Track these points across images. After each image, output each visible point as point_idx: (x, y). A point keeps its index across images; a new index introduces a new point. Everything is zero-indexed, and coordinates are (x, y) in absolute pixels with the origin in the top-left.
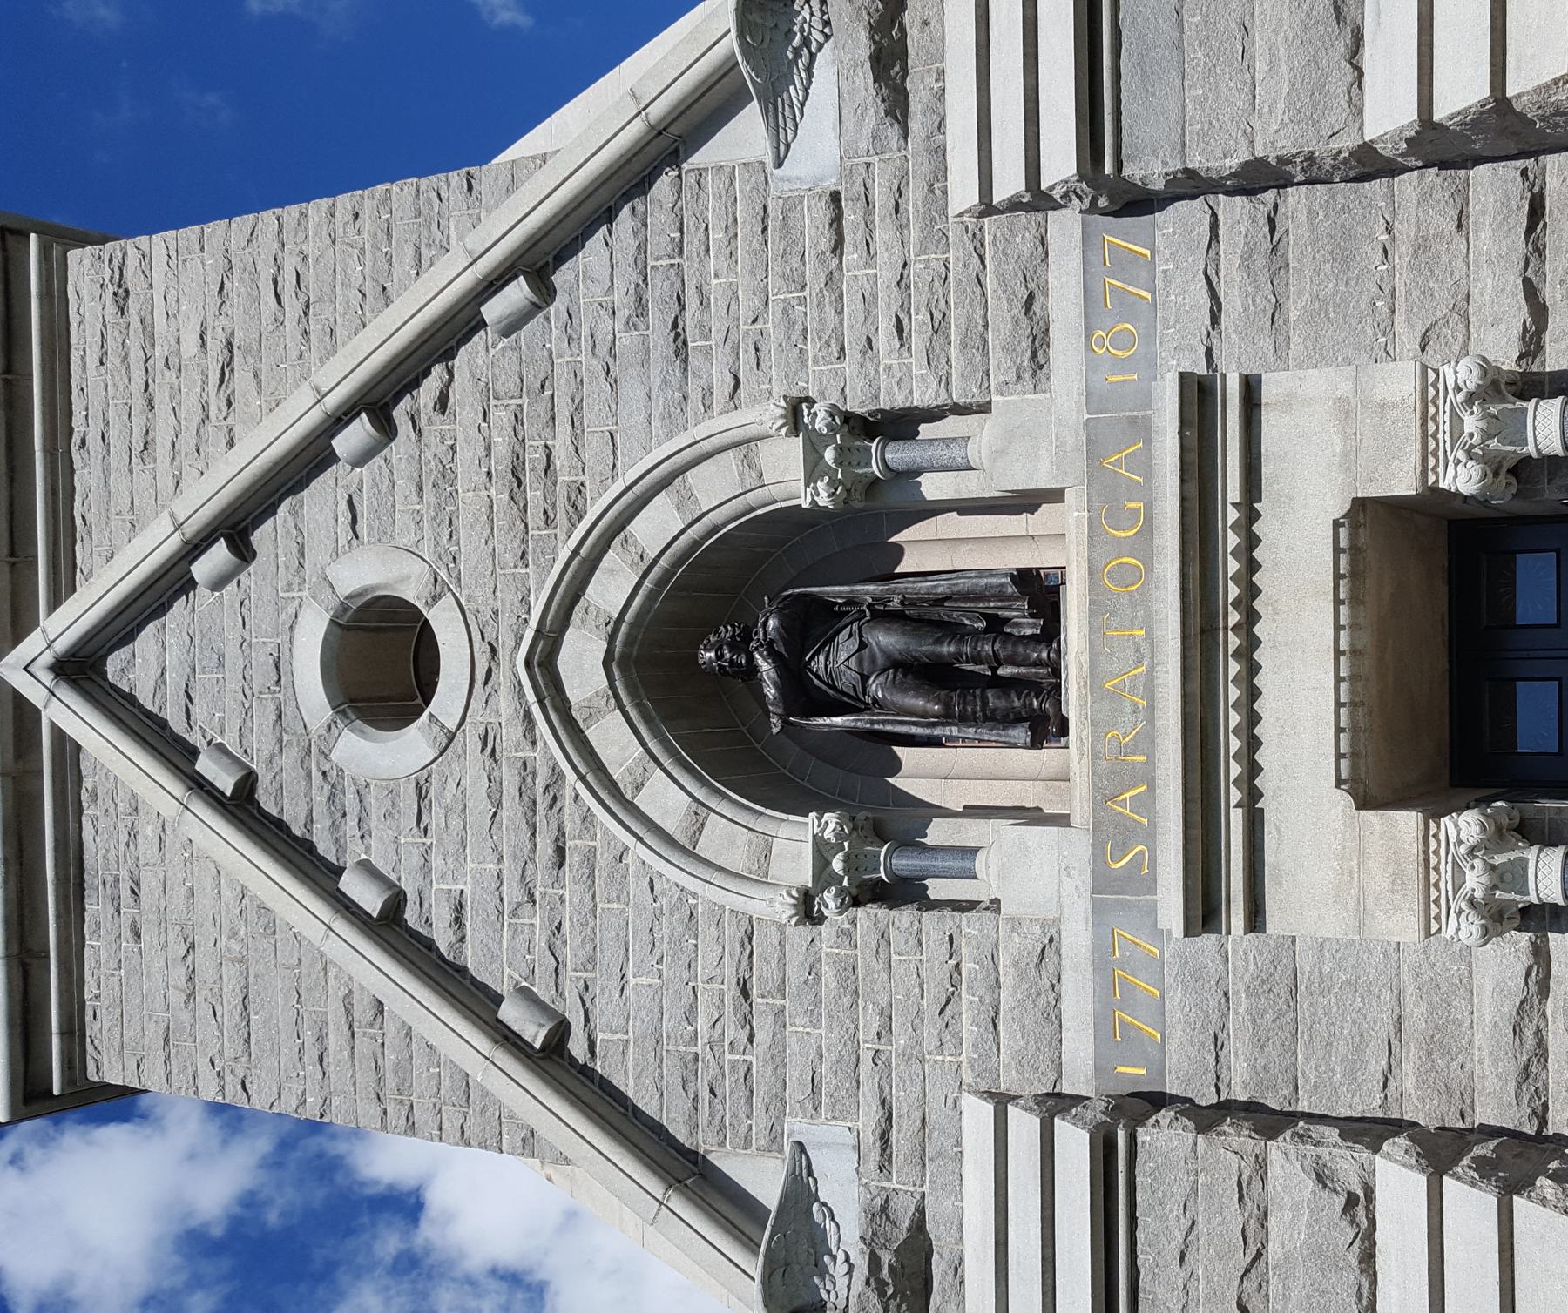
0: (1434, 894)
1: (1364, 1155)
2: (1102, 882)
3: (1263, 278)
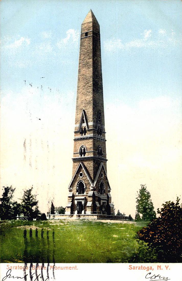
2: (77, 195)
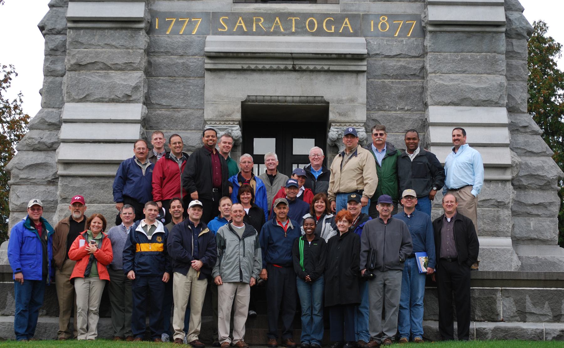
0: (218, 123)
1: (142, 100)
2: (215, 15)
3: (398, 72)
